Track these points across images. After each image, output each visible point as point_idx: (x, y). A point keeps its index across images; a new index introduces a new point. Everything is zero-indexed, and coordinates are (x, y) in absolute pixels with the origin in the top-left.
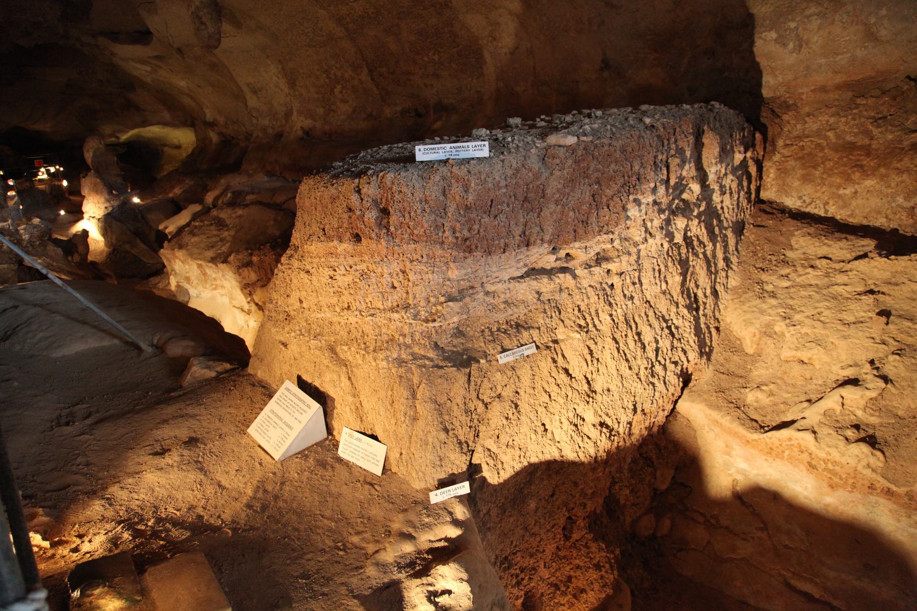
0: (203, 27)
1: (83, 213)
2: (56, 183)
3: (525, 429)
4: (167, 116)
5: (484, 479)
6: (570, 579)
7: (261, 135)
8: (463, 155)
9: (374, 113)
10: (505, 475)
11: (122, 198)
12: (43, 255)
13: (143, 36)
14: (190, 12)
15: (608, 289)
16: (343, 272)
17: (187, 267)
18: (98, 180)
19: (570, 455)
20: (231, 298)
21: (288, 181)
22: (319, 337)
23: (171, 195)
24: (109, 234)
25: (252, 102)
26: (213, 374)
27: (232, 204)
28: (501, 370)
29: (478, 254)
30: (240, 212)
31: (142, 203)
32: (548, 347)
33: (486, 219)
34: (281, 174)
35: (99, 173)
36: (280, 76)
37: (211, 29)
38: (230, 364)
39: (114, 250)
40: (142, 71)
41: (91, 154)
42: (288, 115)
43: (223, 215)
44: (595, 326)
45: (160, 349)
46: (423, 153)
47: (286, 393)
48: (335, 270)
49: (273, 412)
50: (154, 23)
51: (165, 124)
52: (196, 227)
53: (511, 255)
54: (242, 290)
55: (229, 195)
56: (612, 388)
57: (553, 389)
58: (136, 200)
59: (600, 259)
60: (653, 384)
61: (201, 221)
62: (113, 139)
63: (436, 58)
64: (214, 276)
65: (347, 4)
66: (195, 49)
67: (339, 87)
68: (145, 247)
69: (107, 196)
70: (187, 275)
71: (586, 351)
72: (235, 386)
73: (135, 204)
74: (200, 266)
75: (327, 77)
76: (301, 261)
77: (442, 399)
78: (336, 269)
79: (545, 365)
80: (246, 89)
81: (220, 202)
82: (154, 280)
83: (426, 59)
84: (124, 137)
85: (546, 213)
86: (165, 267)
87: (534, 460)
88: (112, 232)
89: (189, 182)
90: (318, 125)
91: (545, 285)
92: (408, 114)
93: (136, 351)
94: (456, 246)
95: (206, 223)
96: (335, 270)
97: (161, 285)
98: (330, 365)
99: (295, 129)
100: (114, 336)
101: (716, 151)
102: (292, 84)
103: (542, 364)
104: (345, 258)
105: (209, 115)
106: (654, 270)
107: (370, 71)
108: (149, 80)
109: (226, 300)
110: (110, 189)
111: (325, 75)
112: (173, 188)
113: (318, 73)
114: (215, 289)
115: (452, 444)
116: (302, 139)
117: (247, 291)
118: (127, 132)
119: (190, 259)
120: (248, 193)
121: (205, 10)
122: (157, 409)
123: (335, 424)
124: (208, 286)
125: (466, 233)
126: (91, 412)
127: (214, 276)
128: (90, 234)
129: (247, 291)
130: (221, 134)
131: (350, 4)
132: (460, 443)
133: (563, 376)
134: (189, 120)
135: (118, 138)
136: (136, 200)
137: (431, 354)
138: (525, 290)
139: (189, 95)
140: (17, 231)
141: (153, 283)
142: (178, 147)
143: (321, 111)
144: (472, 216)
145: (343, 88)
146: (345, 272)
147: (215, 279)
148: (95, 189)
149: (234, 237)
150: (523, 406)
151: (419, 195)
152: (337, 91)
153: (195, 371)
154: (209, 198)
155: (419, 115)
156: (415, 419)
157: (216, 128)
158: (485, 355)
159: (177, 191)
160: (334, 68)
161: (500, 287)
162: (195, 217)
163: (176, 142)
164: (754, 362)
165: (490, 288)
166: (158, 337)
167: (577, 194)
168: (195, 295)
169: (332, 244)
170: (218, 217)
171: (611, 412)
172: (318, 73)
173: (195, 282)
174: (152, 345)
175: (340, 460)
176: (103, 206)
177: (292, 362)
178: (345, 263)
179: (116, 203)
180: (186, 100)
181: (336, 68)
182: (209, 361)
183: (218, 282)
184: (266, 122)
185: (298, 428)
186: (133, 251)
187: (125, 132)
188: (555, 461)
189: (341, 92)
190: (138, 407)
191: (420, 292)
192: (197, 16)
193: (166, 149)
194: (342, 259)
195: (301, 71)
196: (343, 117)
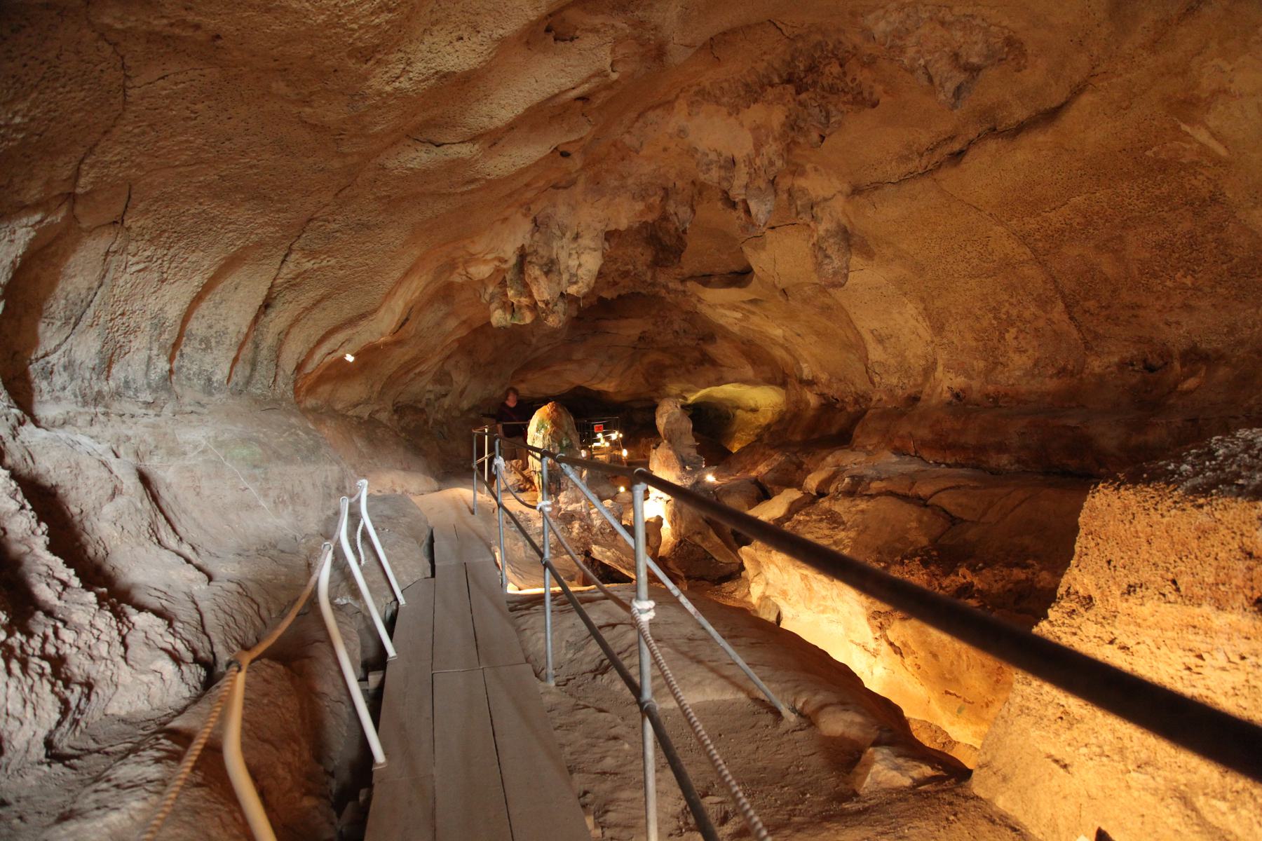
0: (827, 261)
2: (616, 453)
4: (749, 371)
7: (885, 398)
9: (1070, 367)
11: (696, 476)
12: (613, 546)
13: (741, 276)
14: (810, 245)
16: (1222, 661)
17: (786, 577)
18: (671, 452)
20: (848, 629)
21: (928, 463)
22: (1150, 769)
23: (754, 474)
24: (678, 522)
25: (876, 353)
26: (907, 782)
27: (850, 493)
30: (863, 505)
31: (717, 482)
34: (916, 452)
36: (920, 318)
38: (933, 768)
39: (681, 542)
40: (729, 319)
41: (665, 420)
42: (929, 370)
43: (838, 508)
45: (808, 719)
48: (1200, 657)
51: (745, 382)
52: (799, 522)
54: (868, 620)
55: (847, 480)
58: (710, 478)
61: (808, 514)
63: (1188, 281)
64: (824, 593)
65: (1039, 215)
66: (806, 288)
67: (1013, 331)
68: (719, 541)
69: (679, 473)
70: (785, 588)
72: (955, 815)
73: (713, 487)
74: (804, 578)
75: (995, 318)
76: (1102, 626)
78: (1205, 656)
80: (868, 337)
81: (832, 489)
82: (728, 586)
83: (1169, 283)
86: (743, 569)
88: (681, 518)
89: (778, 458)
90: (976, 384)
92: (1130, 368)
93: (770, 716)
95: (814, 517)
96: (1200, 657)
97: (738, 595)
98: (1184, 829)
99: (939, 390)
100: (740, 688)
102: (938, 328)
104: (1229, 639)
105: (807, 372)
107: (1067, 306)
108: (736, 329)
109: (839, 630)
111: (991, 316)
112: (755, 464)
113: (979, 313)
114: (823, 612)
116: (950, 403)
117: (876, 623)
118: (696, 392)
119: (791, 567)
120: (872, 480)
121: (831, 241)
122: (829, 829)
124: (813, 606)
126: (726, 813)
127: (824, 593)
129: (876, 623)
130: (821, 395)
131: (1043, 214)
134: (779, 377)
135: (685, 398)
136: (710, 478)
139: (782, 346)
140: (589, 514)
141: (728, 590)
142: (754, 410)
143: (980, 365)
145: (1021, 331)
146: (1224, 663)
147: (824, 598)
149: (854, 540)
153: (879, 772)
154: (812, 482)
155: (1150, 369)
157: (815, 387)
159: (762, 469)
160: (1007, 304)
163: (752, 404)
164: (361, 418)
166: (804, 699)
168: (790, 616)
169: (1197, 610)
170: (830, 510)
172: (979, 313)
173: (794, 598)
174: (794, 710)
177: (1083, 800)
178: (1227, 648)
180: (779, 353)
181: (1011, 304)
182: (899, 756)
183: (829, 603)
184: (894, 381)
186: (703, 545)
189: (1016, 338)
190: (796, 819)
192: (820, 248)
193: (739, 412)
194: (1221, 641)
195: (953, 311)
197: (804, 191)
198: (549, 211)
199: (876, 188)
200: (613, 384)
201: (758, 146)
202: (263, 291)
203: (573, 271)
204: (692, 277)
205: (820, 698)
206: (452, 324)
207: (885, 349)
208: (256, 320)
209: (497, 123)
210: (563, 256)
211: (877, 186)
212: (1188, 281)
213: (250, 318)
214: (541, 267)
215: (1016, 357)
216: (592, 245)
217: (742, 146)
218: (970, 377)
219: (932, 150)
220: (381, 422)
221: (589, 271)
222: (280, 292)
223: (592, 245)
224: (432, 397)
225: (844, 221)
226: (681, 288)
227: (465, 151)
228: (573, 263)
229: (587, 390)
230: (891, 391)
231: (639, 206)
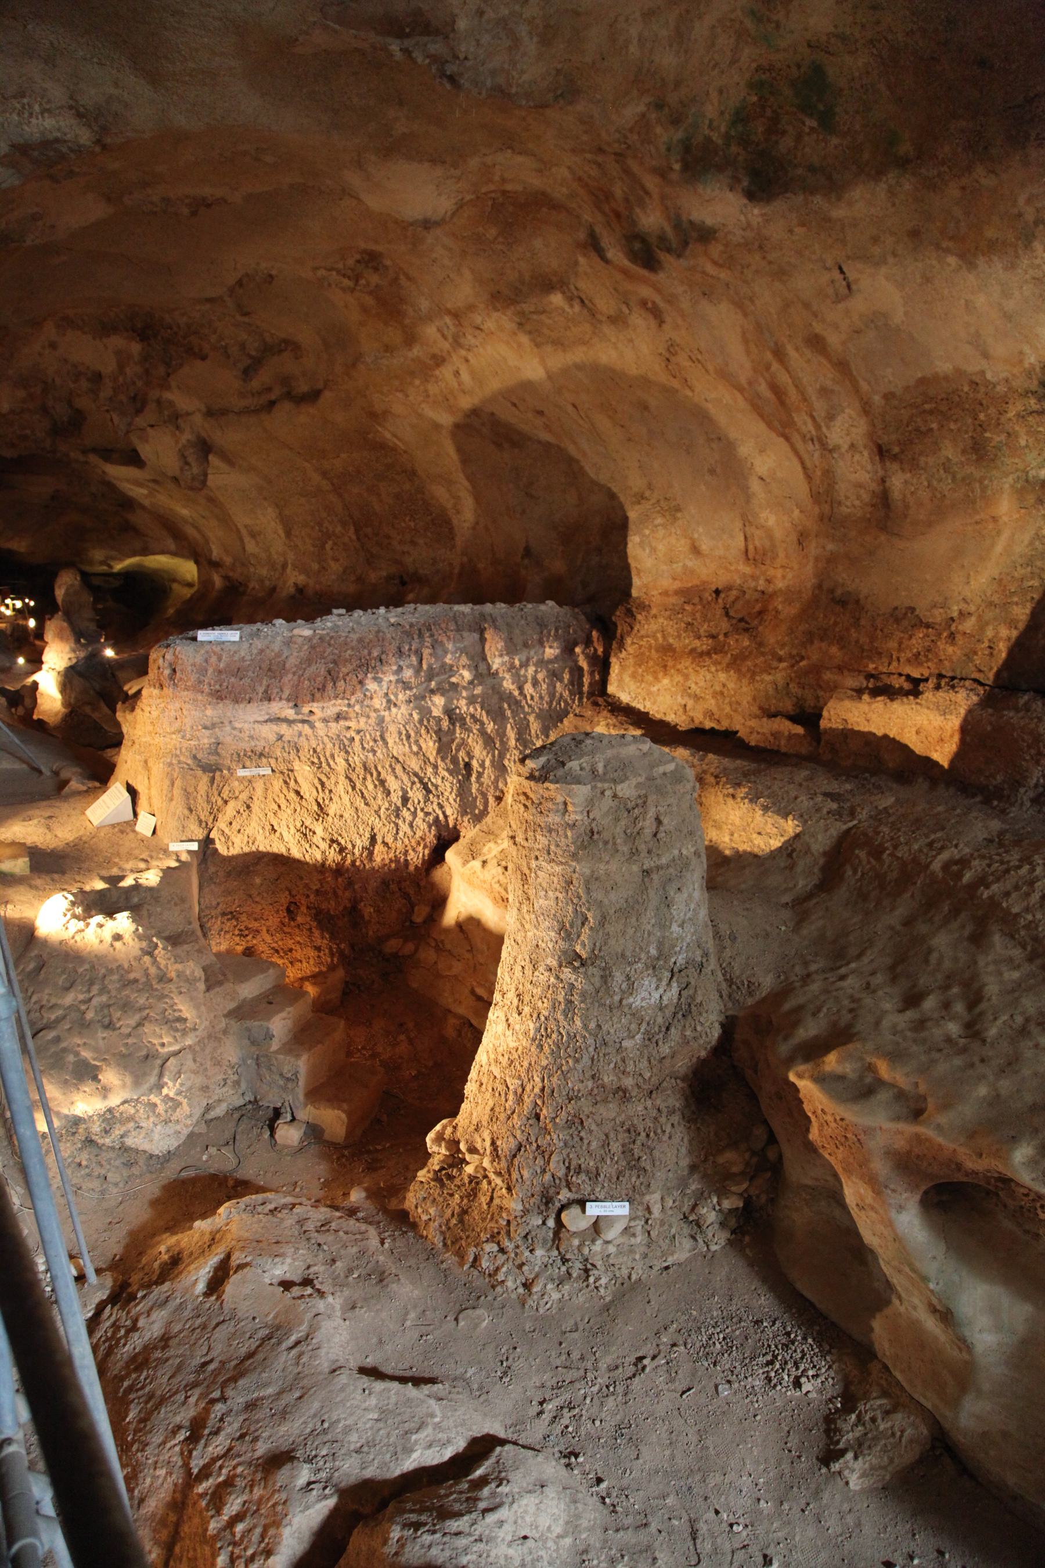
1: (42, 663)
2: (21, 622)
3: (253, 824)
4: (172, 545)
5: (216, 850)
6: (291, 950)
8: (224, 639)
10: (234, 851)
13: (134, 459)
15: (347, 743)
18: (65, 624)
19: (296, 853)
25: (251, 547)
28: (241, 780)
29: (227, 702)
32: (282, 773)
33: (233, 679)
35: (68, 617)
37: (195, 470)
39: (71, 712)
40: (138, 493)
44: (329, 765)
45: (56, 773)
46: (203, 635)
50: (145, 451)
51: (175, 554)
53: (253, 706)
56: (346, 815)
57: (283, 804)
58: (109, 653)
59: (338, 717)
60: (397, 825)
62: (105, 568)
63: (412, 524)
67: (330, 543)
71: (316, 781)
73: (109, 660)
77: (191, 790)
79: (277, 784)
80: (244, 532)
82: (109, 752)
84: (118, 567)
85: (286, 680)
87: (261, 849)
91: (284, 729)
94: (211, 694)
100: (24, 761)
101: (501, 645)
102: (288, 534)
103: (275, 783)
106: (400, 733)
110: (79, 635)
115: (193, 817)
116: (293, 597)
123: (139, 810)
128: (40, 687)
130: (226, 578)
132: (200, 822)
133: (292, 795)
134: (197, 555)
135: (111, 567)
136: (109, 653)
137: (190, 762)
138: (269, 732)
145: (335, 544)
148: (61, 636)
150: (255, 807)
151: (191, 661)
152: (328, 546)
156: (171, 800)
158: (229, 769)
161: (246, 726)
165: (238, 725)
167: (313, 668)
171: (344, 834)
175: (134, 831)
176: (67, 657)
179: (82, 654)
180: (190, 531)
185: (113, 807)
187: (121, 560)
188: (282, 855)
191: (188, 722)
197: (171, 404)
199: (223, 414)
200: (23, 544)
201: (121, 367)
204: (94, 450)
207: (257, 543)
211: (224, 412)
212: (412, 524)
215: (332, 563)
218: (308, 576)
219: (259, 393)
225: (203, 434)
230: (261, 581)
231: (21, 394)
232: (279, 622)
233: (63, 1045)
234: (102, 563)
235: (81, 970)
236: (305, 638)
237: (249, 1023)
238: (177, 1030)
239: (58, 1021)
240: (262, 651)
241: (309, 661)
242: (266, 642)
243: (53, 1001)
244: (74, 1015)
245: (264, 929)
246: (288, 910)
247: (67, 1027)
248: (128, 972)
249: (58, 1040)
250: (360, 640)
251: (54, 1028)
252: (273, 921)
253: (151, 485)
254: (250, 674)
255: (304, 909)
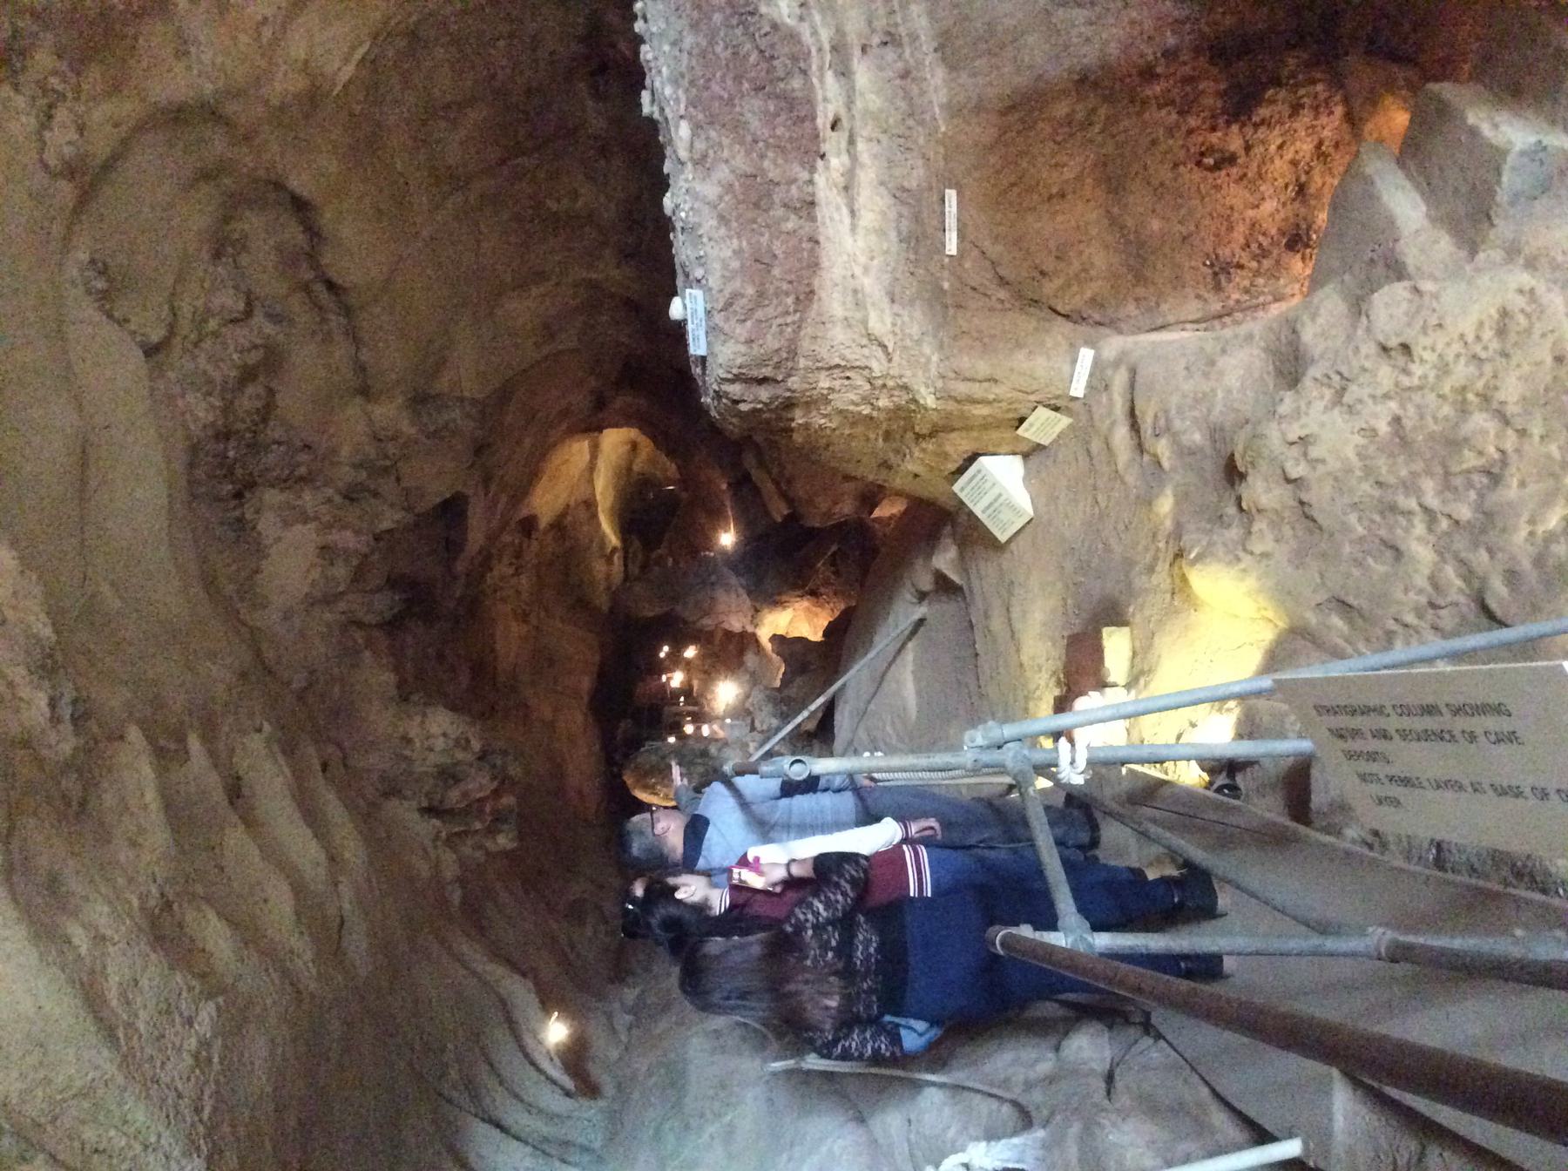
29: (816, 283)
33: (776, 272)
37: (456, 414)
45: (922, 596)
47: (966, 491)
49: (983, 512)
58: (727, 539)
84: (613, 540)
125: (790, 300)
135: (614, 550)
136: (727, 539)
144: (771, 291)
162: (761, 464)
179: (734, 580)
187: (603, 538)
193: (636, 468)
196: (602, 199)
198: (375, 776)
202: (485, 1127)
203: (451, 743)
205: (908, 584)
206: (504, 897)
208: (518, 1138)
209: (322, 857)
210: (433, 758)
213: (515, 1143)
214: (447, 788)
216: (418, 719)
217: (305, 536)
220: (638, 997)
221: (452, 723)
222: (483, 1110)
223: (418, 719)
224: (602, 928)
226: (463, 580)
227: (346, 890)
228: (440, 743)
229: (593, 698)
232: (668, 202)
233: (1526, 564)
234: (609, 560)
235: (1360, 530)
236: (694, 135)
237: (1502, 197)
238: (1528, 331)
239: (1468, 572)
240: (722, 219)
241: (738, 126)
242: (706, 210)
243: (1421, 581)
244: (1460, 544)
245: (1250, 213)
246: (1217, 167)
247: (1483, 555)
248: (1374, 432)
249: (1512, 577)
250: (695, 26)
251: (1484, 580)
252: (1236, 195)
253: (493, 488)
254: (764, 240)
255: (1214, 138)
